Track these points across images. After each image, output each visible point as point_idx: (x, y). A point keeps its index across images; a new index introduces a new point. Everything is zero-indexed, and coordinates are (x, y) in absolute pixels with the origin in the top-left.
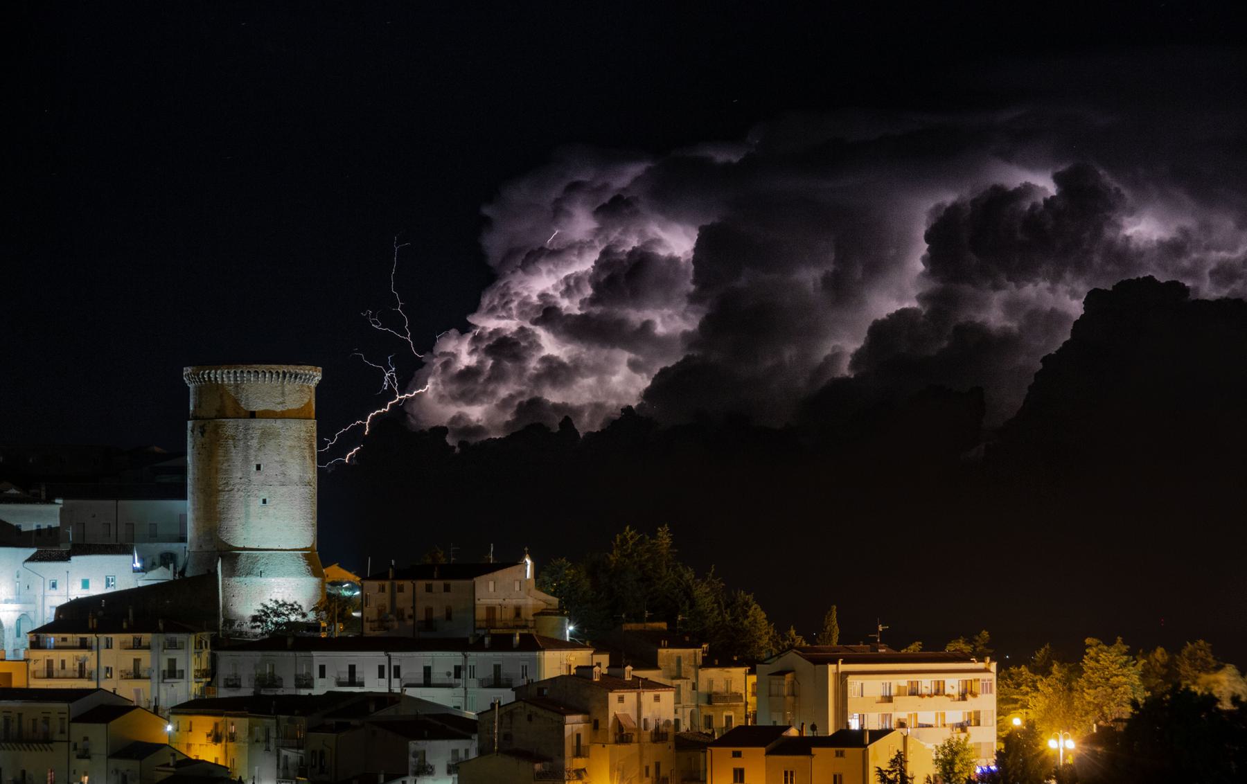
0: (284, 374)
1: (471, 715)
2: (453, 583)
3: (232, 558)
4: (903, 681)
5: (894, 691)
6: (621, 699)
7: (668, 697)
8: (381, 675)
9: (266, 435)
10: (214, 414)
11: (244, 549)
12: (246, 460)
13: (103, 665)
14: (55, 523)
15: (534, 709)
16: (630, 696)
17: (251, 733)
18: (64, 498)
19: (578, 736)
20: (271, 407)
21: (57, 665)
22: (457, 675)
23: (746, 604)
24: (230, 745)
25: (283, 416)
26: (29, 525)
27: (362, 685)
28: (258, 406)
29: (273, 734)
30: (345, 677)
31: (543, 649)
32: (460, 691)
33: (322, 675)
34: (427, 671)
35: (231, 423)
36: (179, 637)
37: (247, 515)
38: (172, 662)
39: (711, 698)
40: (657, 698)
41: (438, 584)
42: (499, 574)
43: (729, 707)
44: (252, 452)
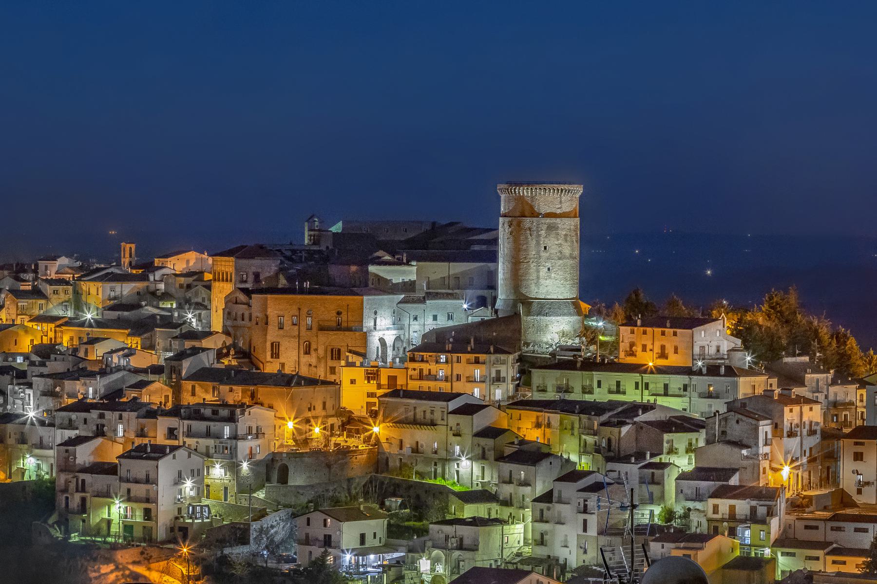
0: (562, 190)
1: (697, 416)
2: (679, 331)
3: (523, 302)
6: (791, 411)
7: (817, 408)
8: (637, 388)
10: (518, 214)
12: (538, 243)
13: (455, 373)
14: (413, 277)
15: (740, 416)
16: (796, 409)
17: (561, 423)
18: (418, 261)
19: (766, 432)
20: (554, 210)
21: (425, 372)
22: (685, 389)
23: (845, 336)
24: (547, 430)
26: (397, 279)
27: (624, 393)
28: (544, 209)
29: (577, 425)
30: (614, 388)
31: (739, 376)
32: (686, 399)
33: (599, 386)
34: (666, 386)
35: (528, 220)
36: (503, 357)
38: (498, 372)
39: (835, 404)
40: (811, 409)
41: (669, 331)
42: (707, 326)
43: (846, 409)
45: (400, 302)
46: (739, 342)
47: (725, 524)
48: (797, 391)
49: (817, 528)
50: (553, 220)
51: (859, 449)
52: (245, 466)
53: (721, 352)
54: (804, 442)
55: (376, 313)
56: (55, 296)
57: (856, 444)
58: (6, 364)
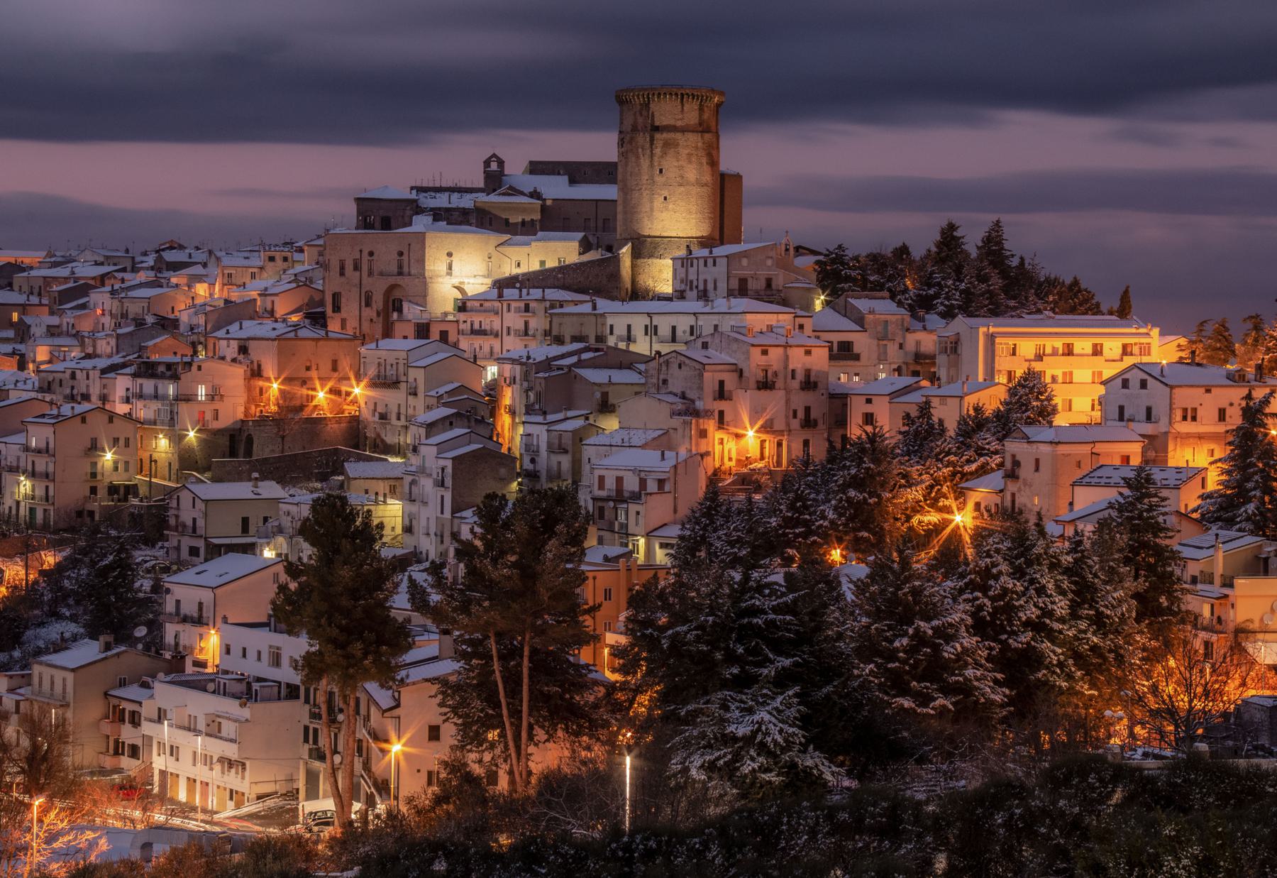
4: (1059, 344)
5: (1048, 351)
8: (656, 327)
9: (667, 145)
11: (649, 237)
12: (652, 165)
20: (672, 122)
25: (683, 130)
37: (652, 209)
44: (656, 159)
50: (671, 135)
52: (192, 435)
53: (774, 287)
55: (450, 255)
56: (271, 264)
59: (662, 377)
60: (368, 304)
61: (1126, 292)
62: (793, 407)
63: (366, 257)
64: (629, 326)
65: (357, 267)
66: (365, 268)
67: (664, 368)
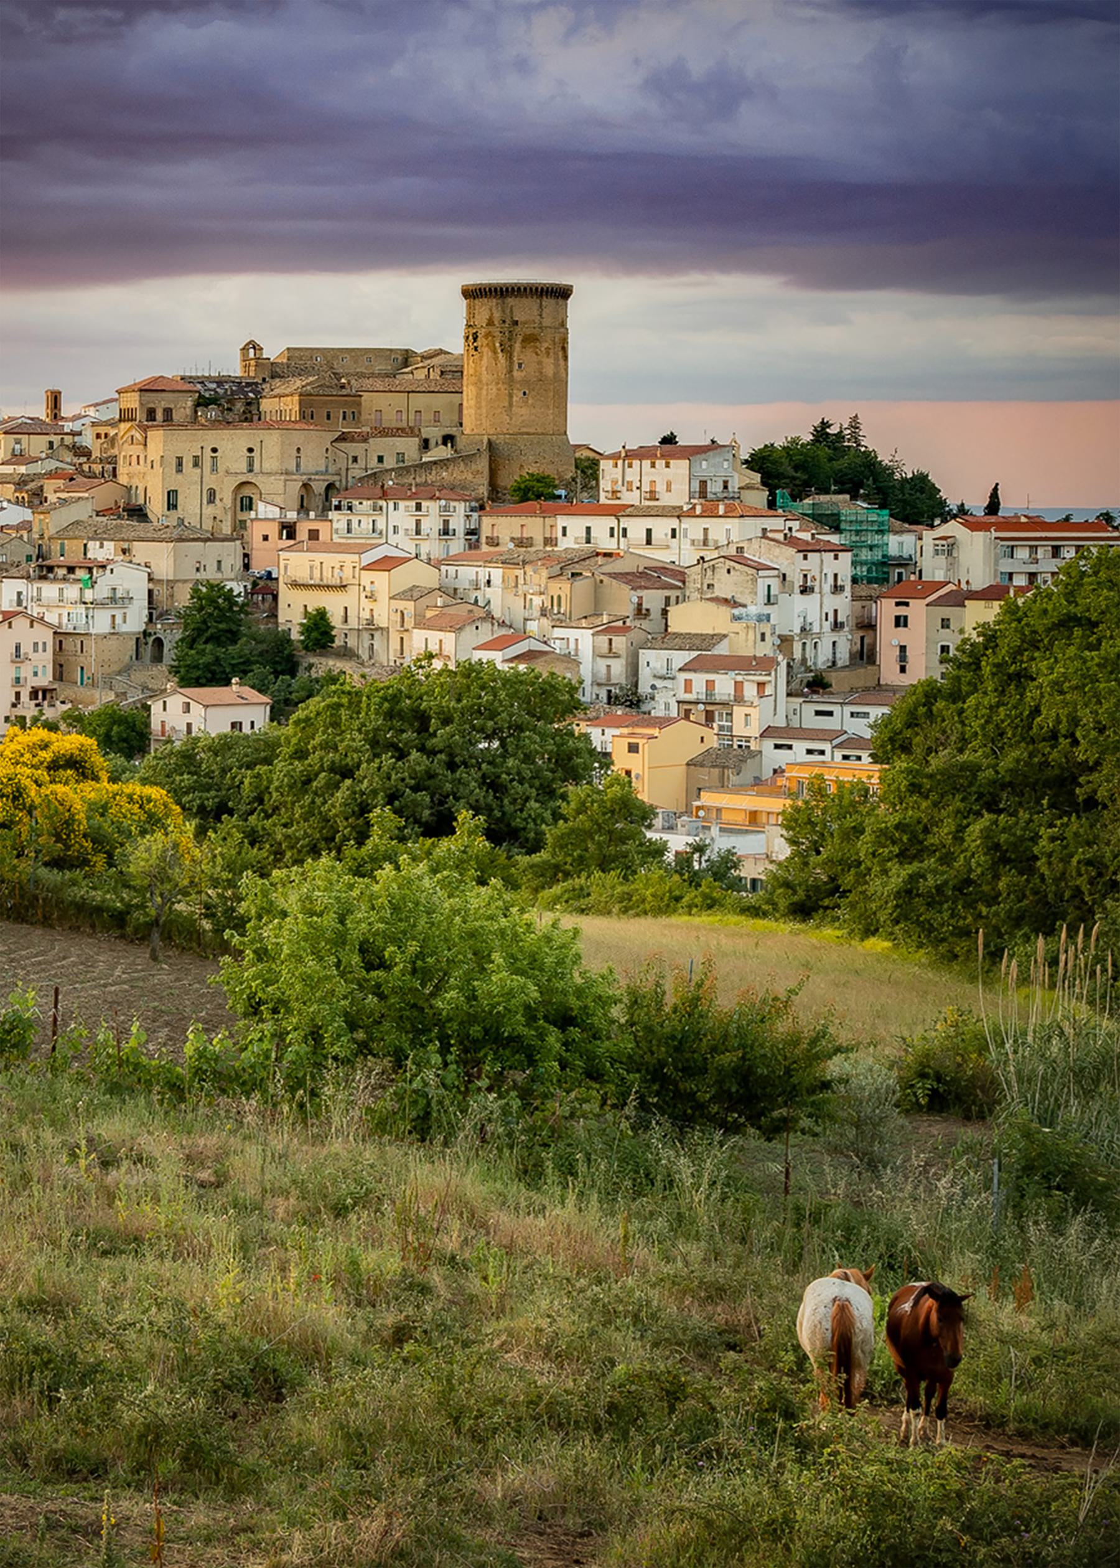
22: (674, 536)
45: (336, 440)
46: (757, 477)
47: (701, 707)
48: (518, 396)
49: (830, 714)
51: (902, 611)
54: (825, 600)
57: (898, 604)
58: (640, 593)
59: (707, 582)
60: (211, 500)
61: (996, 489)
62: (825, 610)
63: (208, 453)
64: (588, 529)
65: (197, 462)
66: (207, 463)
67: (709, 573)
